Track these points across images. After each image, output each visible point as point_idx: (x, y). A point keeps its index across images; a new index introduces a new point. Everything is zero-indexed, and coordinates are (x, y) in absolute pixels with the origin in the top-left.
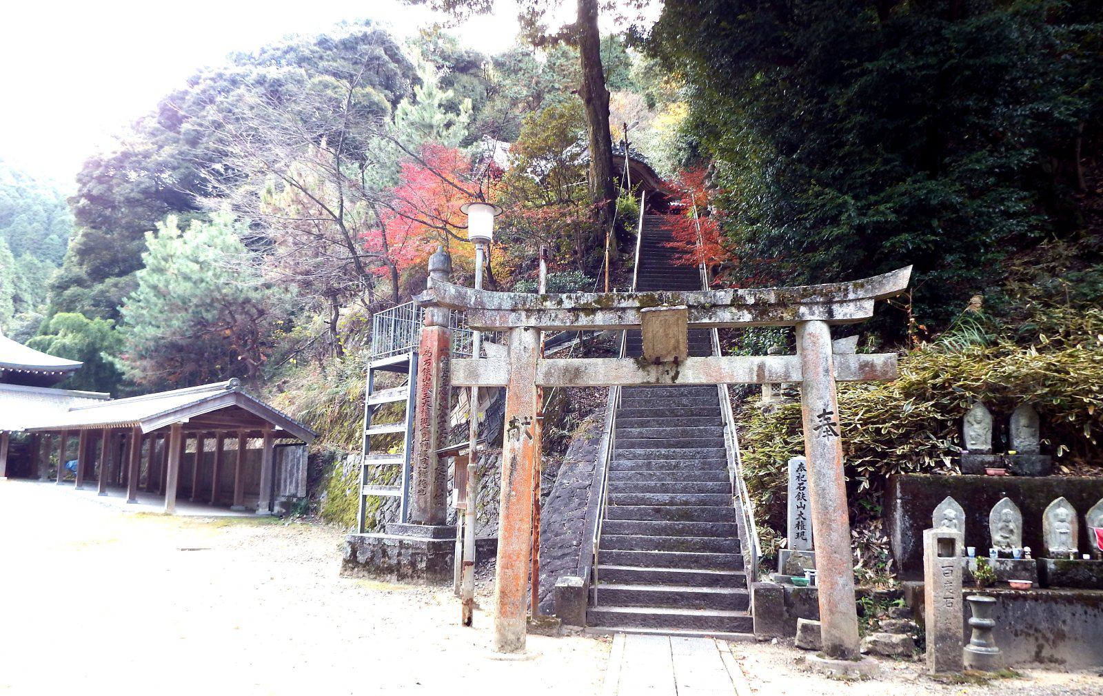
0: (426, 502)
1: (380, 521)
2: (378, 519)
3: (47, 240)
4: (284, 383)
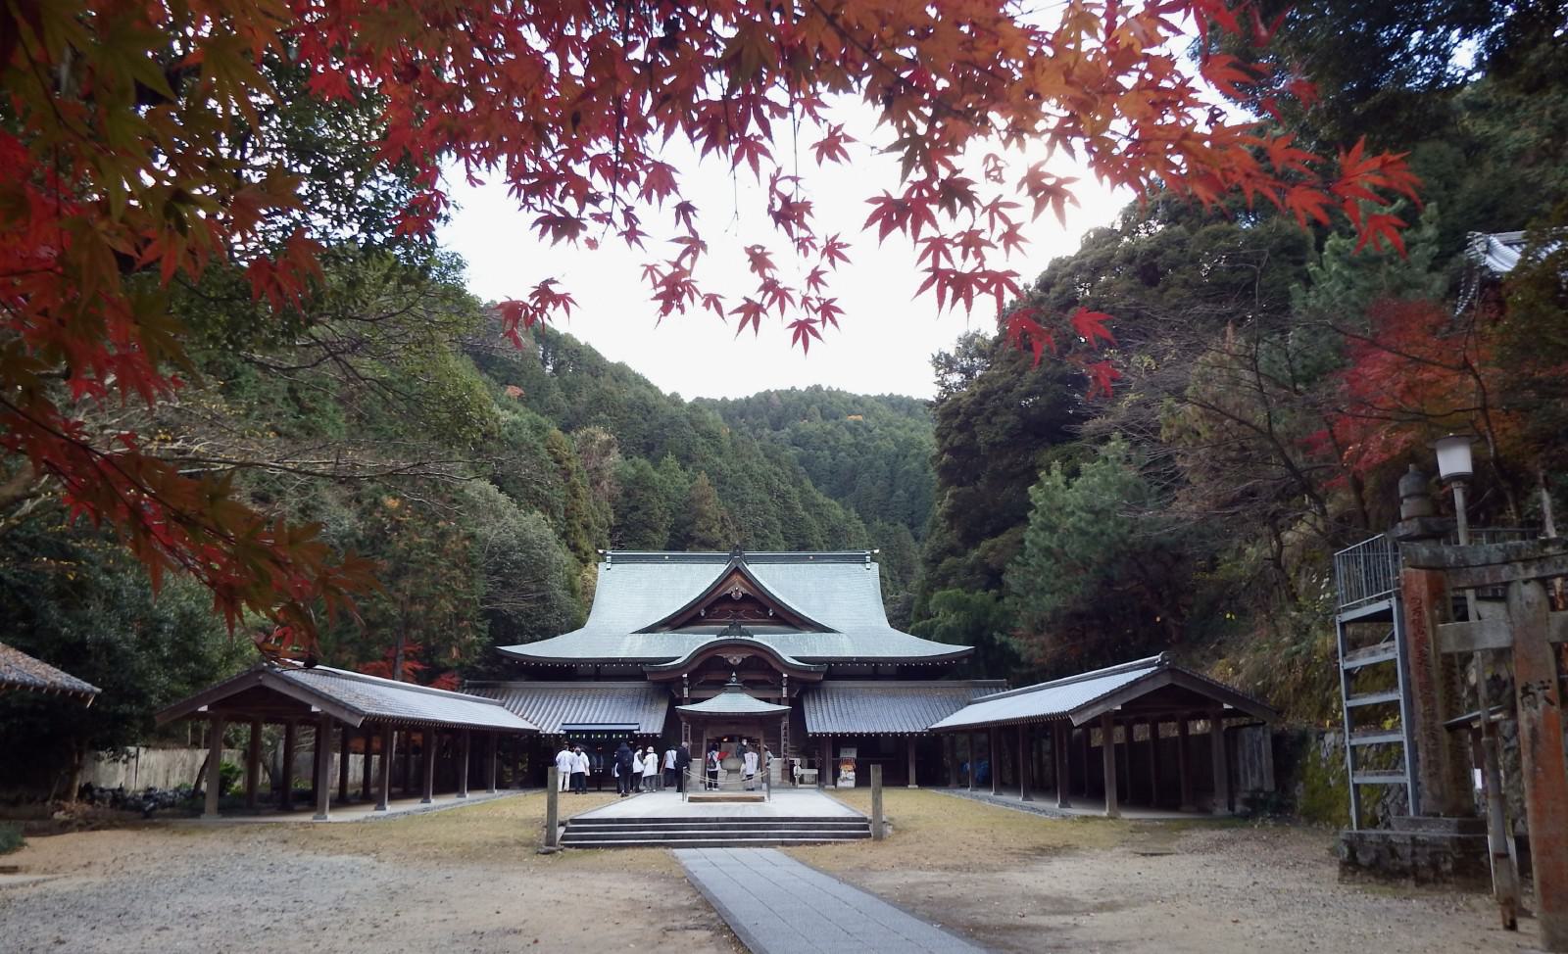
0: (1441, 788)
1: (1383, 818)
2: (1381, 814)
3: (894, 499)
4: (1219, 643)
